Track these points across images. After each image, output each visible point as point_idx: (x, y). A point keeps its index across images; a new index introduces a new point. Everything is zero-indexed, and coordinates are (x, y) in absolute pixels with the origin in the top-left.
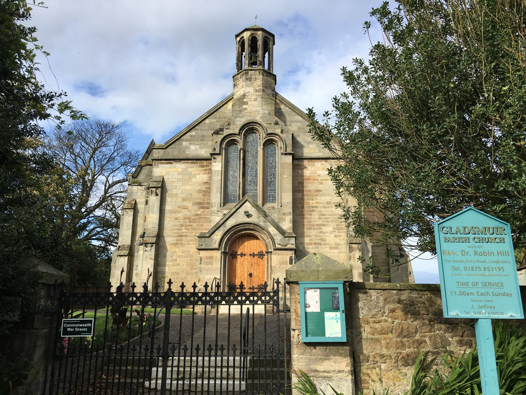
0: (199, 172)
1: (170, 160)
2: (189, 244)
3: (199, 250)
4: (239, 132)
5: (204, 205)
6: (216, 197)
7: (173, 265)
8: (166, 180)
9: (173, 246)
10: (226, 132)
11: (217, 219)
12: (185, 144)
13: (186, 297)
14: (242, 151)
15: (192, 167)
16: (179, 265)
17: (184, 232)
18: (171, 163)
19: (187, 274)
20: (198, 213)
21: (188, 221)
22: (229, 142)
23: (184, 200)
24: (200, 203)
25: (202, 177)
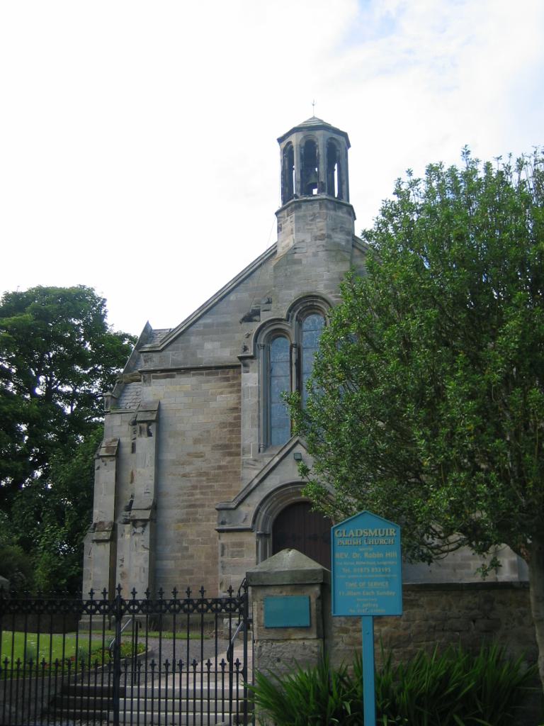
0: (220, 390)
1: (169, 373)
2: (208, 520)
3: (220, 531)
4: (288, 316)
5: (231, 449)
6: (250, 435)
7: (183, 557)
8: (163, 407)
9: (181, 524)
10: (265, 317)
11: (251, 474)
12: (194, 340)
13: (207, 604)
14: (294, 349)
15: (208, 382)
16: (192, 557)
17: (198, 499)
18: (172, 377)
19: (207, 573)
20: (223, 463)
21: (204, 478)
22: (274, 331)
23: (196, 441)
24: (226, 446)
25: (225, 399)
